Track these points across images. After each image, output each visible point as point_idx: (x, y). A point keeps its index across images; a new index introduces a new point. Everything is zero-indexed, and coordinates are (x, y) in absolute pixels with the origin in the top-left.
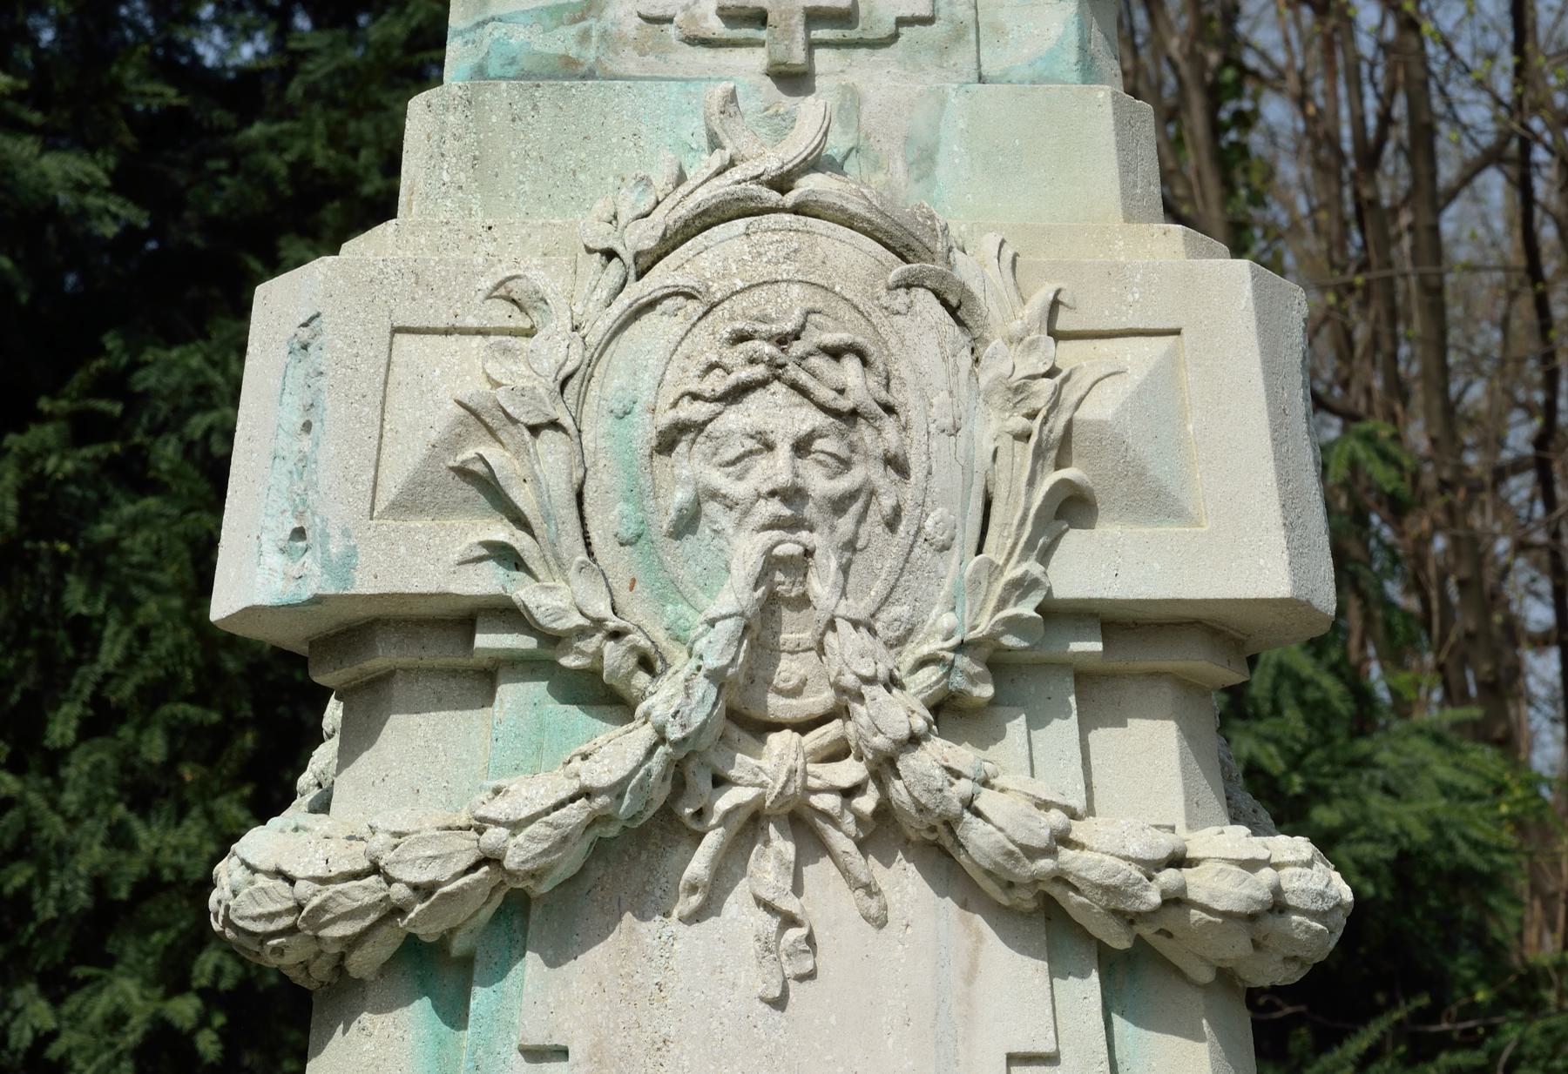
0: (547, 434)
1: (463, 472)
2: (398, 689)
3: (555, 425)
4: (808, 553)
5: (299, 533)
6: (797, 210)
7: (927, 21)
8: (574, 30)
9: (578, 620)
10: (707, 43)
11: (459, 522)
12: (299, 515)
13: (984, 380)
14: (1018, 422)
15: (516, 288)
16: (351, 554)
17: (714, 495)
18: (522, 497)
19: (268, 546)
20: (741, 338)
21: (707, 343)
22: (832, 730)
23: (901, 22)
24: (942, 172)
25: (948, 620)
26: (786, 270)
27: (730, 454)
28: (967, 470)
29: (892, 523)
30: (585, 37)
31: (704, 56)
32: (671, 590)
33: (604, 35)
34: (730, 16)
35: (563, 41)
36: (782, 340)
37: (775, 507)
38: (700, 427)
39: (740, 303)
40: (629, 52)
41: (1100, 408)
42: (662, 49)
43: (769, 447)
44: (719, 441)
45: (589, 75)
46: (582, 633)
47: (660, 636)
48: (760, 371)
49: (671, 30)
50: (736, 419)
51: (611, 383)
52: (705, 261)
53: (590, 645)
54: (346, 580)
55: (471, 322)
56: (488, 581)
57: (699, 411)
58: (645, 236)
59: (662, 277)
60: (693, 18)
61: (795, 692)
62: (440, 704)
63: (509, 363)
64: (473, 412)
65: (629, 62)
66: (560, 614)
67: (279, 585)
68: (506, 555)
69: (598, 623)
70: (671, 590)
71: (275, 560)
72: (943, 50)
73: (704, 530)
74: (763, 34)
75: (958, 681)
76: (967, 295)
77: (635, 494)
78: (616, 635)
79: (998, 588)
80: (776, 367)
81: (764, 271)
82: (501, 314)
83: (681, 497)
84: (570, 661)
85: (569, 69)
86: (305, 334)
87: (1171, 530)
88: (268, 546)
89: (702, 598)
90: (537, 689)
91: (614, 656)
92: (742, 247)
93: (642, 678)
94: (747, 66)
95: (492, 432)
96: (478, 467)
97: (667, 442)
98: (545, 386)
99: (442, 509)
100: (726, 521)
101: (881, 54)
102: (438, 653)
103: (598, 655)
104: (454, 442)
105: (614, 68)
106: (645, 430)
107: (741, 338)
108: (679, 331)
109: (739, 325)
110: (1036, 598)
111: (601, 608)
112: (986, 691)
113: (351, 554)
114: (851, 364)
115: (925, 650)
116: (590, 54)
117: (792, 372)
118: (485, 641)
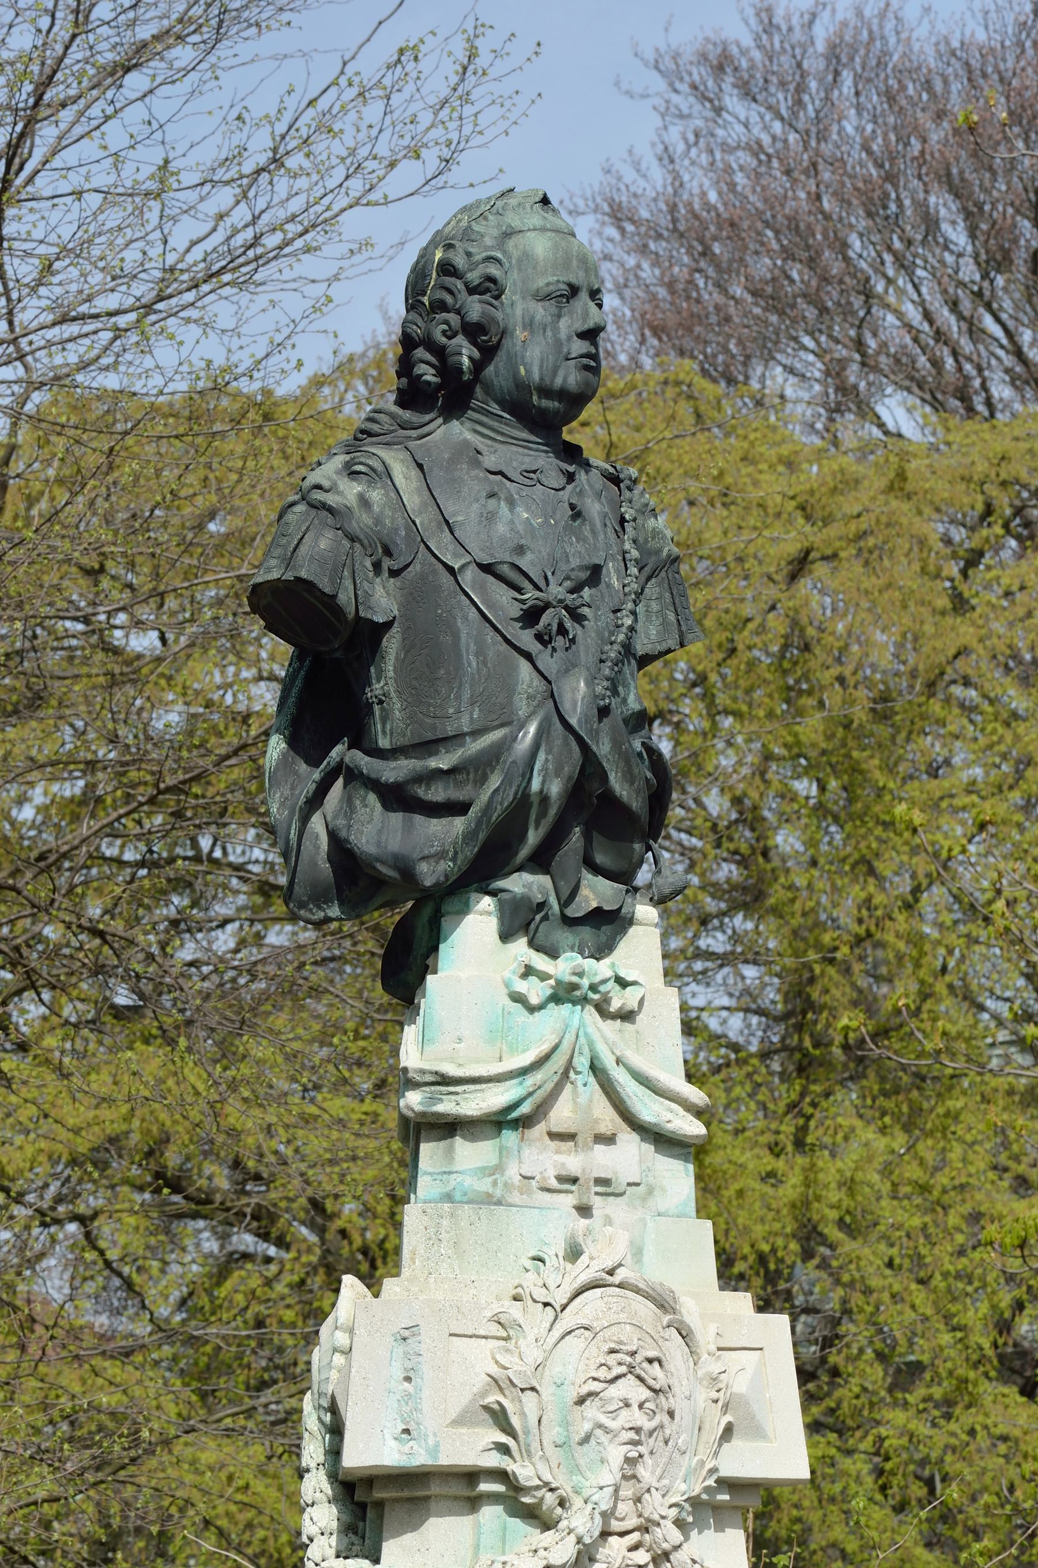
0: (529, 1393)
1: (486, 1408)
2: (433, 1505)
3: (533, 1389)
4: (641, 1456)
5: (407, 1431)
6: (620, 1286)
7: (637, 1184)
8: (490, 1180)
9: (537, 1482)
10: (549, 1190)
11: (480, 1430)
12: (404, 1421)
13: (700, 1374)
14: (714, 1395)
15: (503, 1318)
16: (437, 1445)
17: (600, 1426)
18: (515, 1421)
19: (388, 1436)
20: (612, 1351)
21: (597, 1353)
22: (635, 1537)
23: (629, 1184)
24: (646, 1259)
25: (683, 1487)
26: (623, 1317)
27: (611, 1408)
28: (694, 1417)
29: (666, 1442)
30: (495, 1183)
31: (547, 1196)
32: (577, 1469)
33: (506, 1184)
34: (561, 1179)
35: (484, 1185)
36: (633, 1354)
37: (632, 1435)
38: (597, 1394)
39: (607, 1333)
40: (516, 1193)
41: (740, 1386)
42: (528, 1192)
43: (627, 1405)
44: (605, 1402)
45: (499, 1203)
46: (537, 1488)
47: (569, 1490)
48: (623, 1369)
49: (533, 1182)
50: (615, 1392)
51: (555, 1370)
52: (587, 1310)
53: (539, 1494)
54: (436, 1458)
55: (482, 1333)
56: (493, 1460)
57: (596, 1386)
58: (559, 1298)
59: (568, 1320)
60: (544, 1179)
61: (622, 1519)
62: (450, 1513)
63: (509, 1356)
64: (496, 1381)
65: (515, 1198)
66: (529, 1478)
67: (397, 1456)
68: (504, 1449)
69: (546, 1484)
70: (577, 1469)
71: (393, 1443)
72: (644, 1200)
73: (593, 1442)
74: (573, 1188)
75: (684, 1514)
76: (690, 1332)
77: (566, 1424)
78: (551, 1490)
79: (704, 1472)
80: (631, 1367)
81: (614, 1318)
82: (495, 1330)
83: (587, 1426)
84: (526, 1500)
85: (489, 1200)
86: (406, 1333)
87: (761, 1444)
88: (388, 1436)
89: (588, 1474)
90: (498, 1510)
91: (550, 1499)
92: (600, 1304)
93: (559, 1510)
94: (568, 1201)
95: (501, 1389)
96: (496, 1407)
97: (581, 1401)
98: (529, 1370)
99: (473, 1424)
100: (604, 1438)
101: (619, 1199)
102: (459, 1489)
103: (542, 1499)
104: (484, 1394)
105: (510, 1200)
106: (573, 1395)
107: (612, 1351)
108: (583, 1346)
109: (613, 1345)
110: (715, 1477)
111: (547, 1477)
112: (690, 1519)
113: (437, 1445)
114: (656, 1365)
115: (673, 1500)
116: (498, 1193)
117: (638, 1371)
118: (485, 1487)
